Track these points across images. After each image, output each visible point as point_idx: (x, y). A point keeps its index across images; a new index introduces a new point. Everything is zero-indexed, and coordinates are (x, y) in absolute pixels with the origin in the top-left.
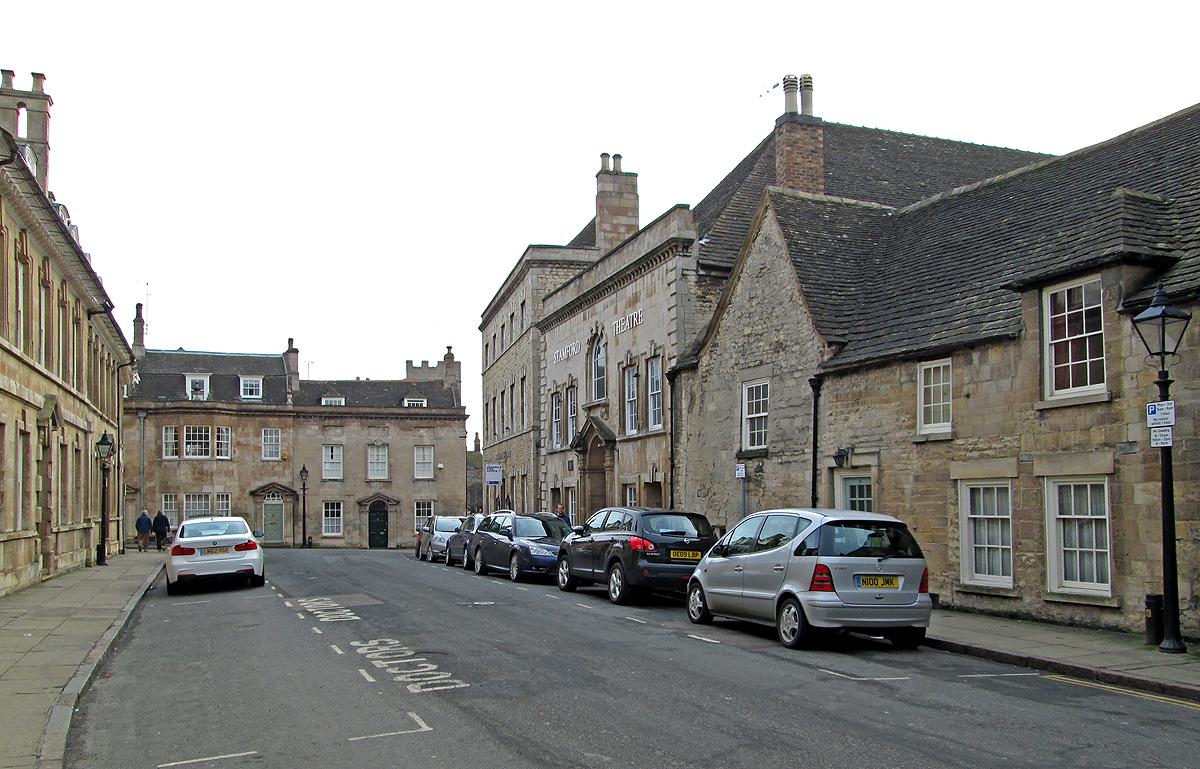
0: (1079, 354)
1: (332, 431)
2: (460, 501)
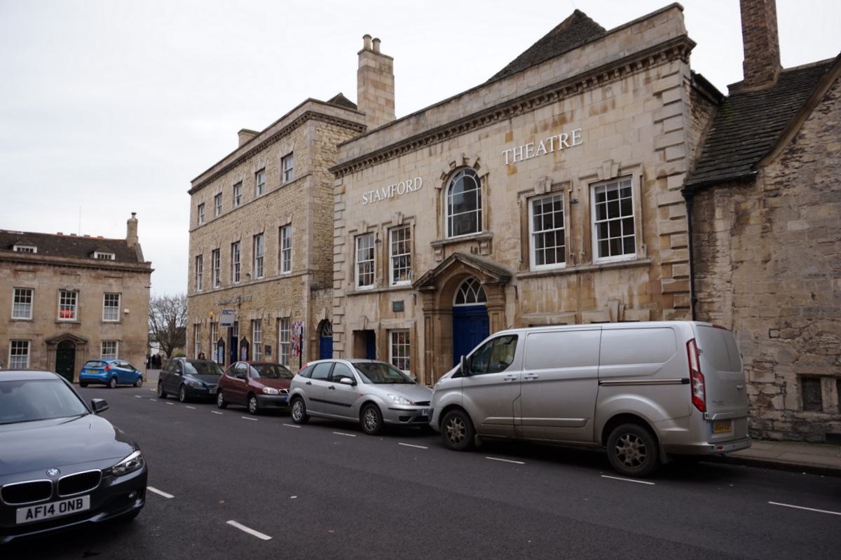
0: (550, 243)
1: (23, 276)
2: (143, 341)
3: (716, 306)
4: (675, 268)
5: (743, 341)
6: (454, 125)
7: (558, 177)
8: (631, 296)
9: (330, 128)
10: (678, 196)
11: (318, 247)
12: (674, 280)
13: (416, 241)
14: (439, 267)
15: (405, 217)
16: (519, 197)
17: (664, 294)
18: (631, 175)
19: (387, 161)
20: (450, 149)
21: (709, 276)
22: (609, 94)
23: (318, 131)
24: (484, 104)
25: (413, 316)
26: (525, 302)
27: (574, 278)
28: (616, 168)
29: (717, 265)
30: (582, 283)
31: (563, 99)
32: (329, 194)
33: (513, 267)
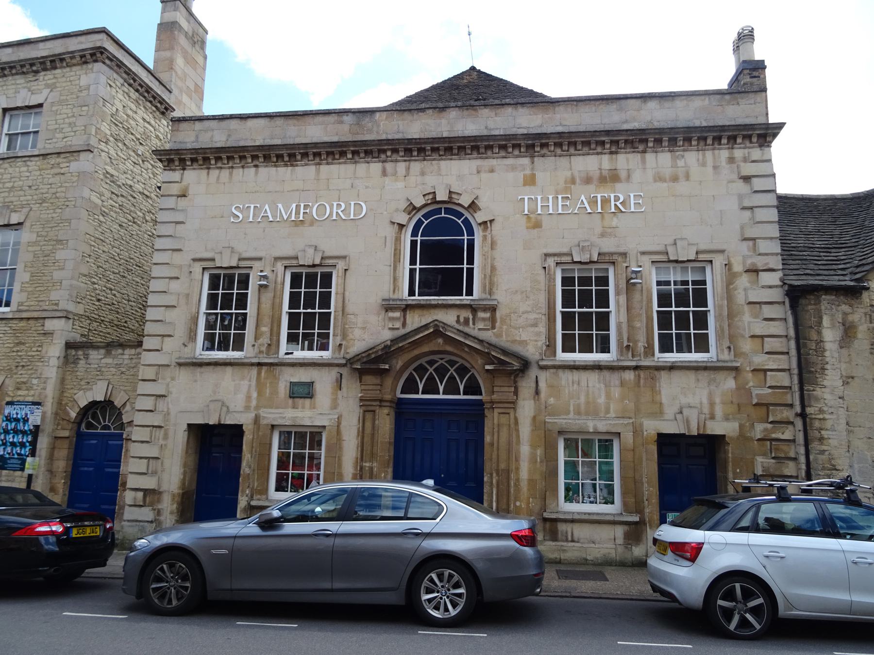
3: (828, 424)
4: (771, 376)
5: (861, 465)
6: (438, 143)
7: (608, 245)
8: (712, 404)
9: (126, 90)
10: (777, 295)
11: (85, 276)
12: (770, 391)
13: (347, 294)
14: (394, 341)
15: (327, 254)
16: (545, 260)
17: (757, 405)
18: (251, 267)
19: (292, 165)
20: (423, 174)
21: (818, 389)
22: (681, 163)
23: (111, 86)
24: (486, 128)
25: (334, 406)
26: (552, 400)
27: (629, 376)
28: (693, 250)
29: (827, 377)
30: (642, 381)
31: (616, 153)
32: (113, 193)
33: (532, 350)
